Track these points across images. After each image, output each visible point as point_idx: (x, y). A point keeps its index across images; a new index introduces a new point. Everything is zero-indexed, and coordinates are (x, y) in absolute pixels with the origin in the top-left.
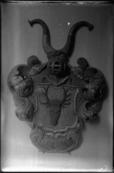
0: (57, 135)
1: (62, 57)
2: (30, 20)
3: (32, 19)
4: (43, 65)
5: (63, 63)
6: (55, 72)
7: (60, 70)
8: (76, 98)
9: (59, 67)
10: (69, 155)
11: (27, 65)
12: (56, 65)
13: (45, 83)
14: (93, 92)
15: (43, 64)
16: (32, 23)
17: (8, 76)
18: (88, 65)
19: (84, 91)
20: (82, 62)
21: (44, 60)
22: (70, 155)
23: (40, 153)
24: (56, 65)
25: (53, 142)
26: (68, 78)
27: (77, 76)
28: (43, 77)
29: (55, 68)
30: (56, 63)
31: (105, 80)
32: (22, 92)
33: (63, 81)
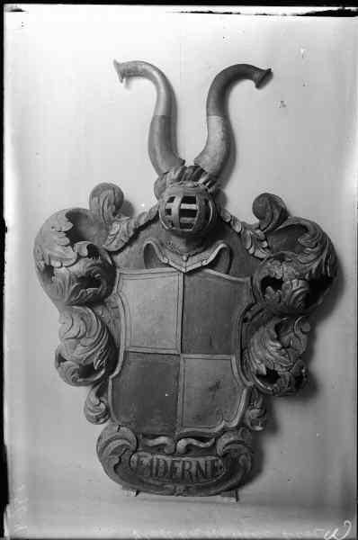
0: (182, 444)
1: (205, 183)
2: (121, 61)
3: (126, 58)
4: (140, 216)
5: (207, 202)
6: (184, 226)
7: (196, 219)
8: (247, 395)
9: (195, 211)
10: (234, 500)
11: (88, 208)
12: (186, 206)
13: (152, 267)
14: (296, 290)
15: (140, 212)
16: (129, 72)
17: (38, 230)
18: (284, 214)
19: (269, 285)
20: (269, 206)
21: (144, 200)
22: (237, 500)
23: (126, 492)
24: (186, 206)
25: (169, 465)
26: (221, 250)
27: (247, 250)
28: (144, 245)
29: (183, 213)
30: (186, 200)
31: (333, 248)
32: (72, 288)
33: (212, 257)
